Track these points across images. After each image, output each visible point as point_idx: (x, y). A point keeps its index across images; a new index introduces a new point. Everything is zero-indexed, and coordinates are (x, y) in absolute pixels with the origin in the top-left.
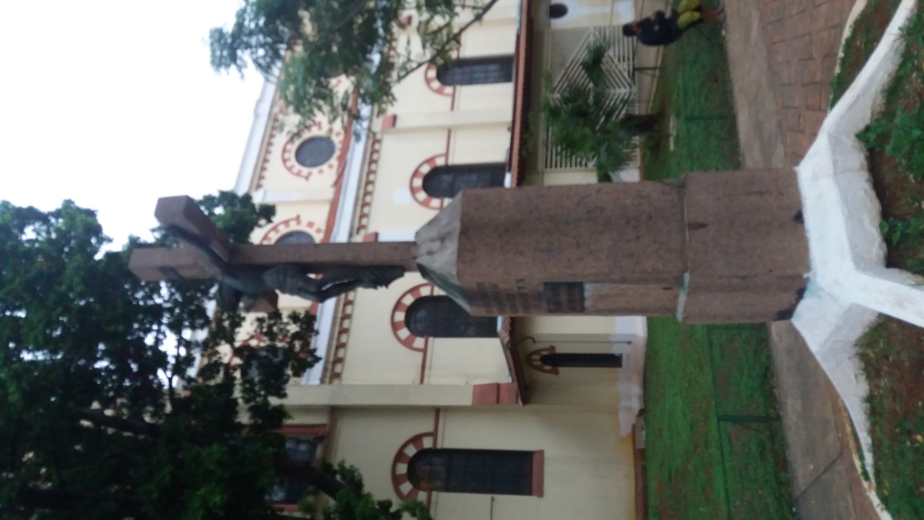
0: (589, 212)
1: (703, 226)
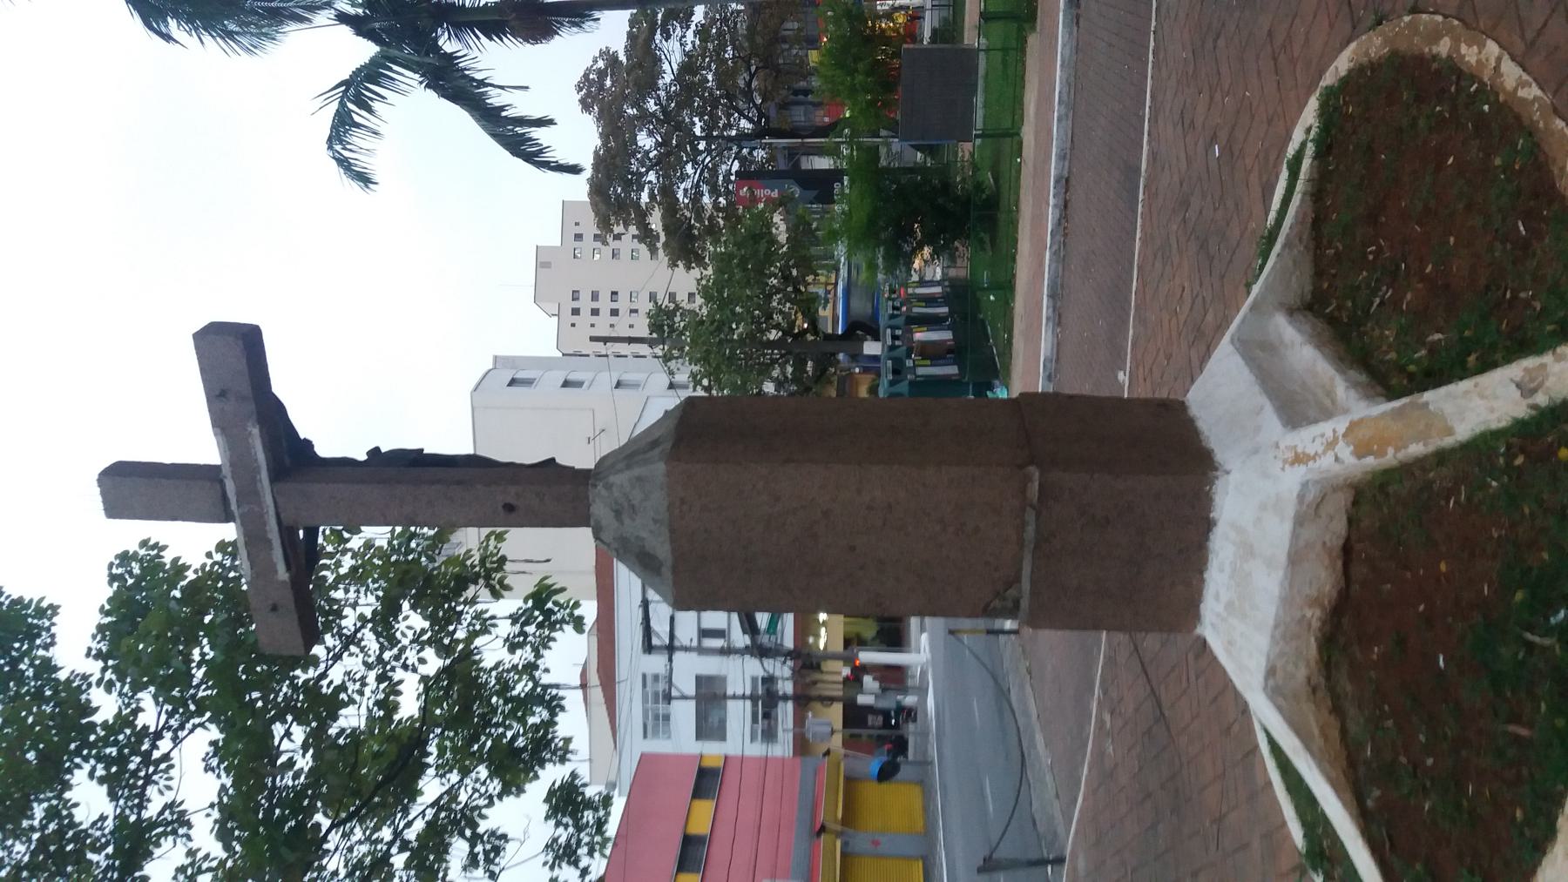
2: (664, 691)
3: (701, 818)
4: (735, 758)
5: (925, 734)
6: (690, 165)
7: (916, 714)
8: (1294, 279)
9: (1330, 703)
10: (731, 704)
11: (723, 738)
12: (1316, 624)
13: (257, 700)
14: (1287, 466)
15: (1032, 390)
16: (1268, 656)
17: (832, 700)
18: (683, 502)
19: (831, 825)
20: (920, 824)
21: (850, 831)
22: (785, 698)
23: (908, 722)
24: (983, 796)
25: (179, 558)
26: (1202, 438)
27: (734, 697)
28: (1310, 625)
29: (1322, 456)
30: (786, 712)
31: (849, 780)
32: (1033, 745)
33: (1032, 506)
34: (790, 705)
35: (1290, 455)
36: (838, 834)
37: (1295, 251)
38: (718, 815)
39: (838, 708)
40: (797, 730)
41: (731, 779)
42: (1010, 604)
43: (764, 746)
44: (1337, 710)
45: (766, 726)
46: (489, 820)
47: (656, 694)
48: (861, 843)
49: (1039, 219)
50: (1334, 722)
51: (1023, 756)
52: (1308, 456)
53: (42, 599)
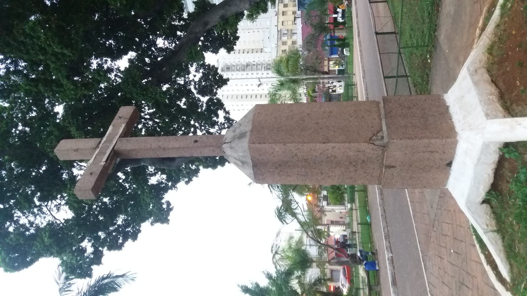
0: (328, 158)
1: (393, 167)
6: (73, 93)
12: (496, 100)
13: (126, 173)
16: (483, 111)
18: (259, 113)
28: (494, 101)
42: (380, 138)
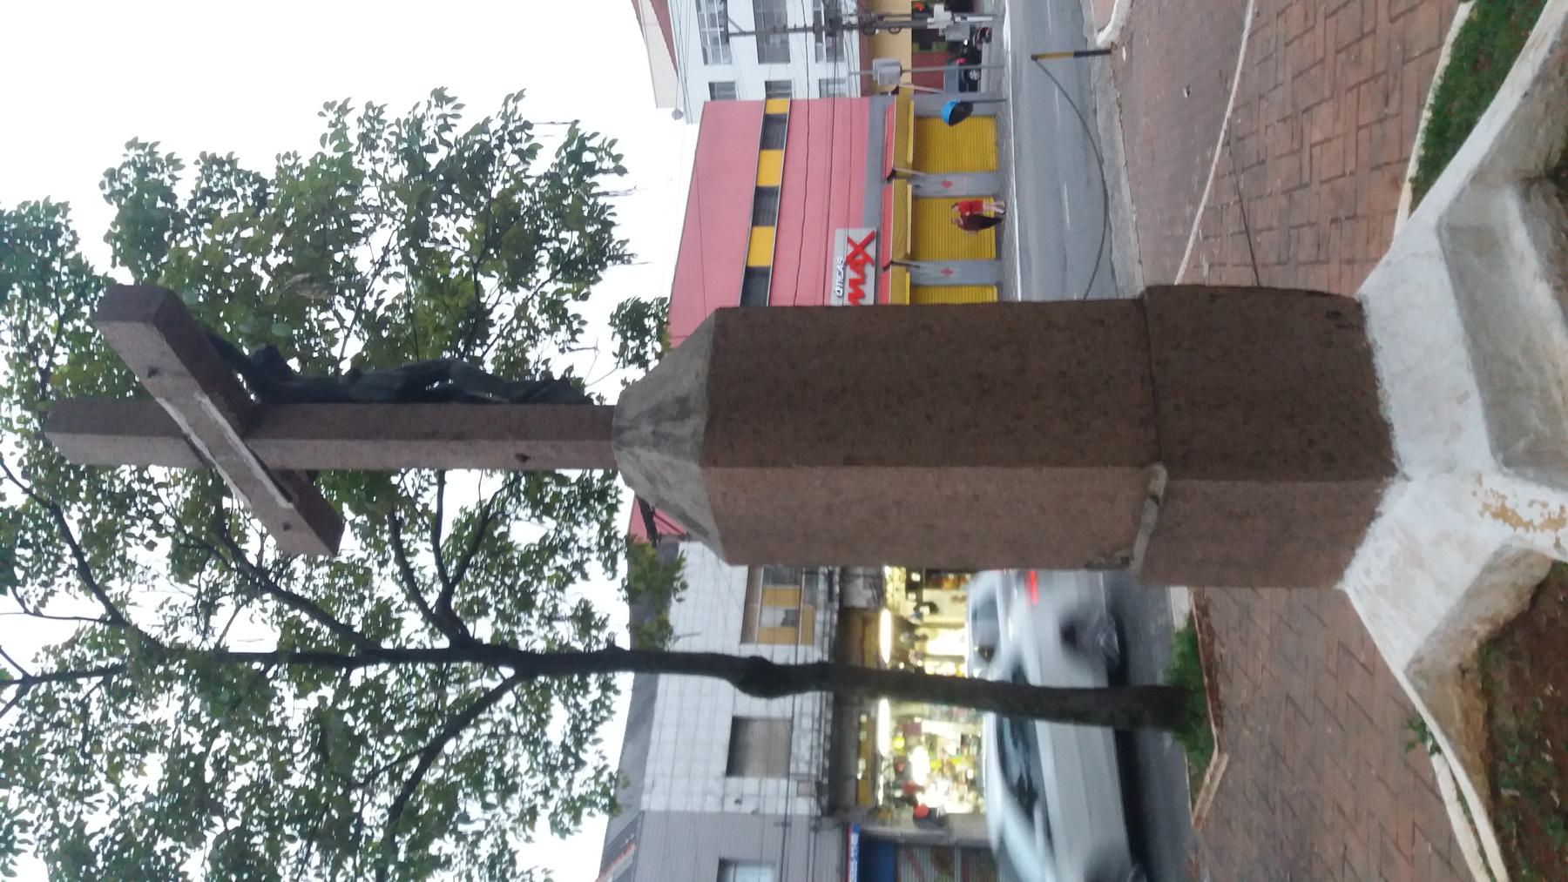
2: (719, 13)
3: (771, 168)
4: (801, 101)
5: (1000, 66)
7: (990, 34)
8: (1541, 131)
9: (1480, 685)
10: (792, 37)
11: (787, 59)
13: (299, 332)
14: (1487, 514)
15: (1169, 282)
17: (901, 26)
19: (902, 170)
20: (992, 161)
21: (921, 174)
22: (850, 27)
23: (981, 43)
24: (1060, 201)
25: (173, 154)
26: (1379, 392)
27: (796, 30)
29: (1539, 532)
30: (852, 41)
31: (919, 118)
32: (1117, 182)
33: (1155, 498)
34: (855, 34)
35: (1495, 503)
36: (909, 178)
37: (1551, 88)
38: (788, 166)
39: (907, 34)
40: (864, 72)
41: (798, 127)
43: (831, 65)
44: (1487, 693)
45: (831, 44)
46: (561, 841)
47: (712, 16)
48: (931, 185)
49: (1217, 767)
50: (1481, 706)
51: (1105, 191)
52: (1519, 519)
53: (47, 199)
